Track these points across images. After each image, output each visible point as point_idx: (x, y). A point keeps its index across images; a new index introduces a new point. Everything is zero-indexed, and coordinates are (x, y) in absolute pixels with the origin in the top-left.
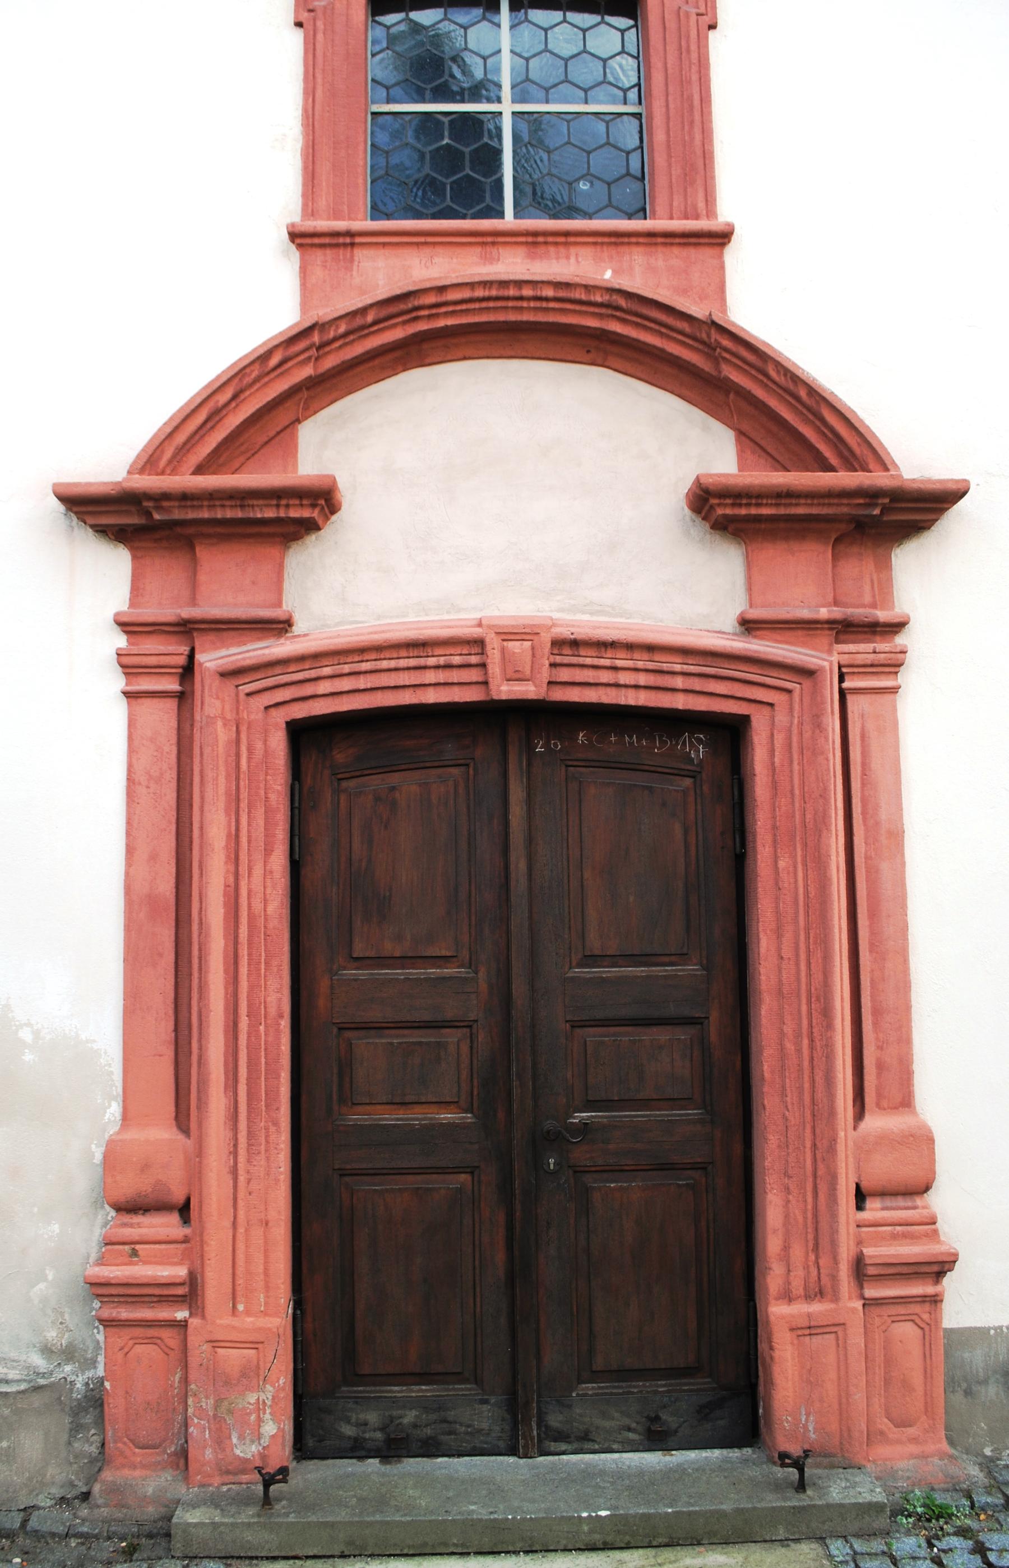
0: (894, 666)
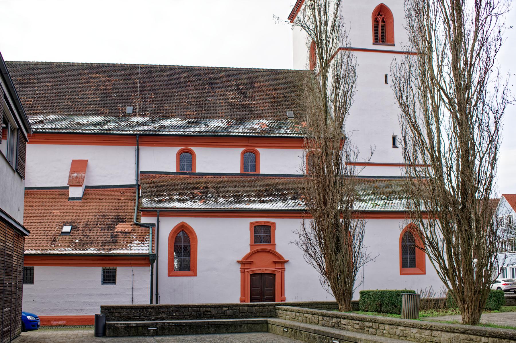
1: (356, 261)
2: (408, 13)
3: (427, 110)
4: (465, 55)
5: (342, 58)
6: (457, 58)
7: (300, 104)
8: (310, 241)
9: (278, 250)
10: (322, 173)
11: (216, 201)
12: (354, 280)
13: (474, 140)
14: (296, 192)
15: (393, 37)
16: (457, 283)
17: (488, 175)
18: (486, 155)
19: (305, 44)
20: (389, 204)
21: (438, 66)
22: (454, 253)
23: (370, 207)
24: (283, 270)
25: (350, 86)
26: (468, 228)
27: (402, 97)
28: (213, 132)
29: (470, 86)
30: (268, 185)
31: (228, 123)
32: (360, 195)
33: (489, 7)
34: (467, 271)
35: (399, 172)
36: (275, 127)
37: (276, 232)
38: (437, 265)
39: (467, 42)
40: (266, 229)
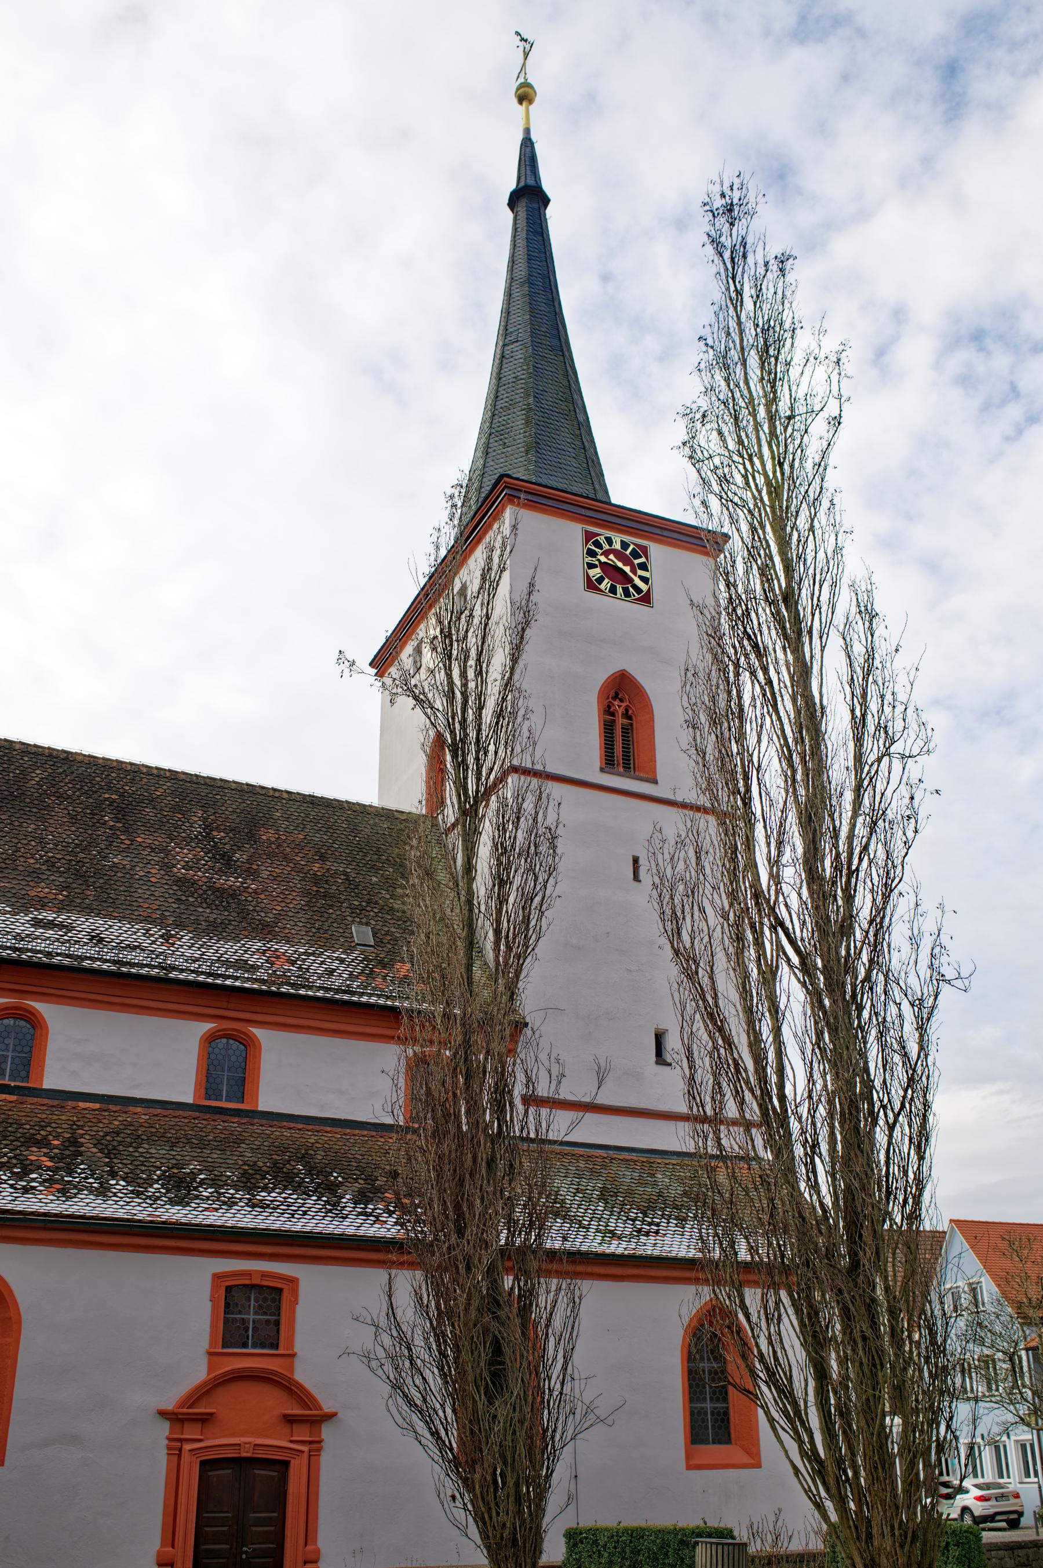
0: (320, 1450)
1: (552, 1425)
2: (690, 712)
3: (746, 976)
4: (836, 846)
5: (520, 797)
6: (816, 849)
7: (392, 909)
8: (410, 1349)
9: (303, 1374)
10: (453, 1130)
11: (103, 1191)
12: (546, 1490)
13: (869, 1075)
14: (370, 1179)
15: (653, 759)
16: (852, 1505)
17: (911, 1175)
18: (901, 1118)
19: (419, 746)
20: (647, 1234)
21: (769, 861)
22: (838, 1407)
23: (592, 1243)
24: (316, 1446)
25: (540, 880)
26: (869, 1333)
27: (679, 934)
28: (114, 962)
29: (851, 927)
30: (282, 1149)
31: (167, 937)
32: (563, 1201)
33: (883, 735)
34: (876, 1468)
35: (676, 1138)
36: (316, 966)
37: (300, 1309)
38: (792, 1447)
39: (836, 815)
40: (265, 1300)
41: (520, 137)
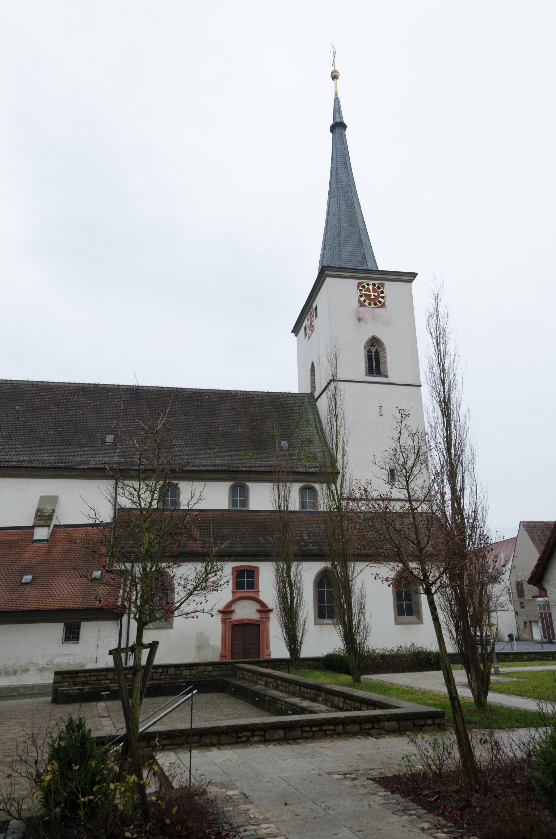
41: (333, 97)
